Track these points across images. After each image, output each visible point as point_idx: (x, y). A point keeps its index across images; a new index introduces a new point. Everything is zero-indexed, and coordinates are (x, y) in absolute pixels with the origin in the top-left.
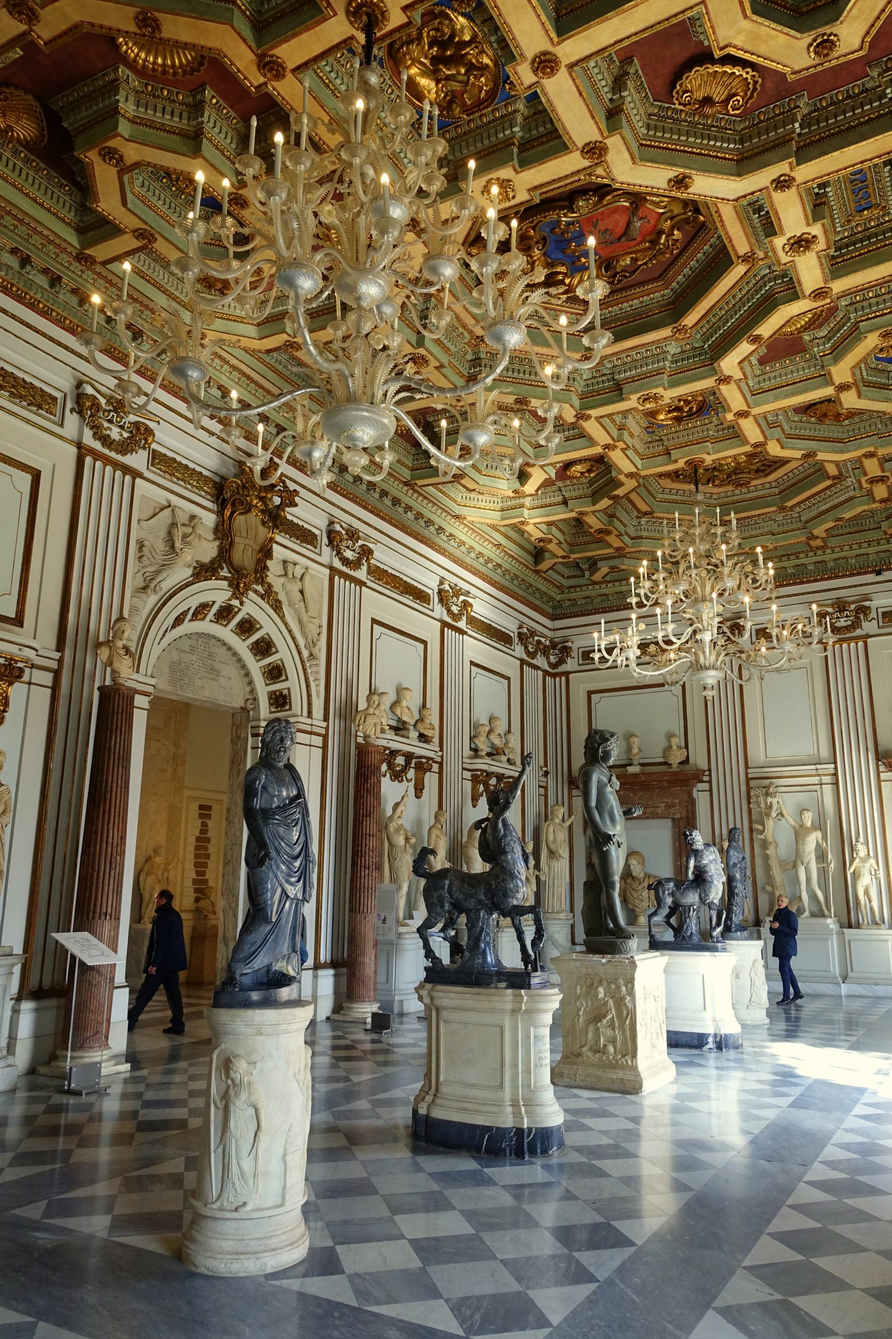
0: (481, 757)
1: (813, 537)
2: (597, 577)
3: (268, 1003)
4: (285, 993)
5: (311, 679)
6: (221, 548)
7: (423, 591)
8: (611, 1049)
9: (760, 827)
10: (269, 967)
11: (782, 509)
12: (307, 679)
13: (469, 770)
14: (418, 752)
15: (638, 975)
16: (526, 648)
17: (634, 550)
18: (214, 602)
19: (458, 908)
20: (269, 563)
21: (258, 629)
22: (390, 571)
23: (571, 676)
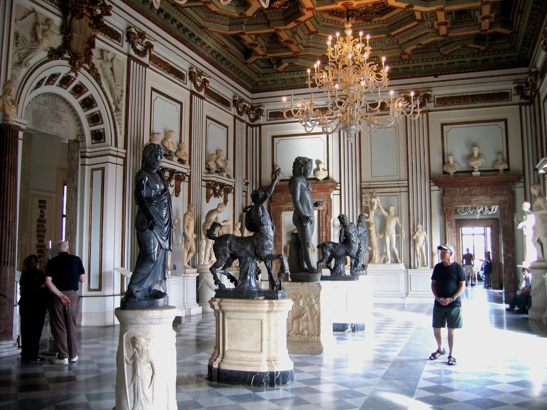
0: (213, 173)
1: (404, 53)
2: (281, 68)
3: (153, 306)
4: (161, 301)
5: (117, 123)
6: (64, 39)
7: (181, 72)
8: (306, 332)
9: (367, 215)
10: (150, 289)
11: (389, 36)
12: (114, 123)
13: (205, 181)
14: (178, 169)
15: (322, 293)
16: (237, 109)
17: (305, 54)
18: (60, 74)
19: (234, 256)
20: (93, 51)
21: (85, 92)
22: (162, 59)
23: (262, 127)
